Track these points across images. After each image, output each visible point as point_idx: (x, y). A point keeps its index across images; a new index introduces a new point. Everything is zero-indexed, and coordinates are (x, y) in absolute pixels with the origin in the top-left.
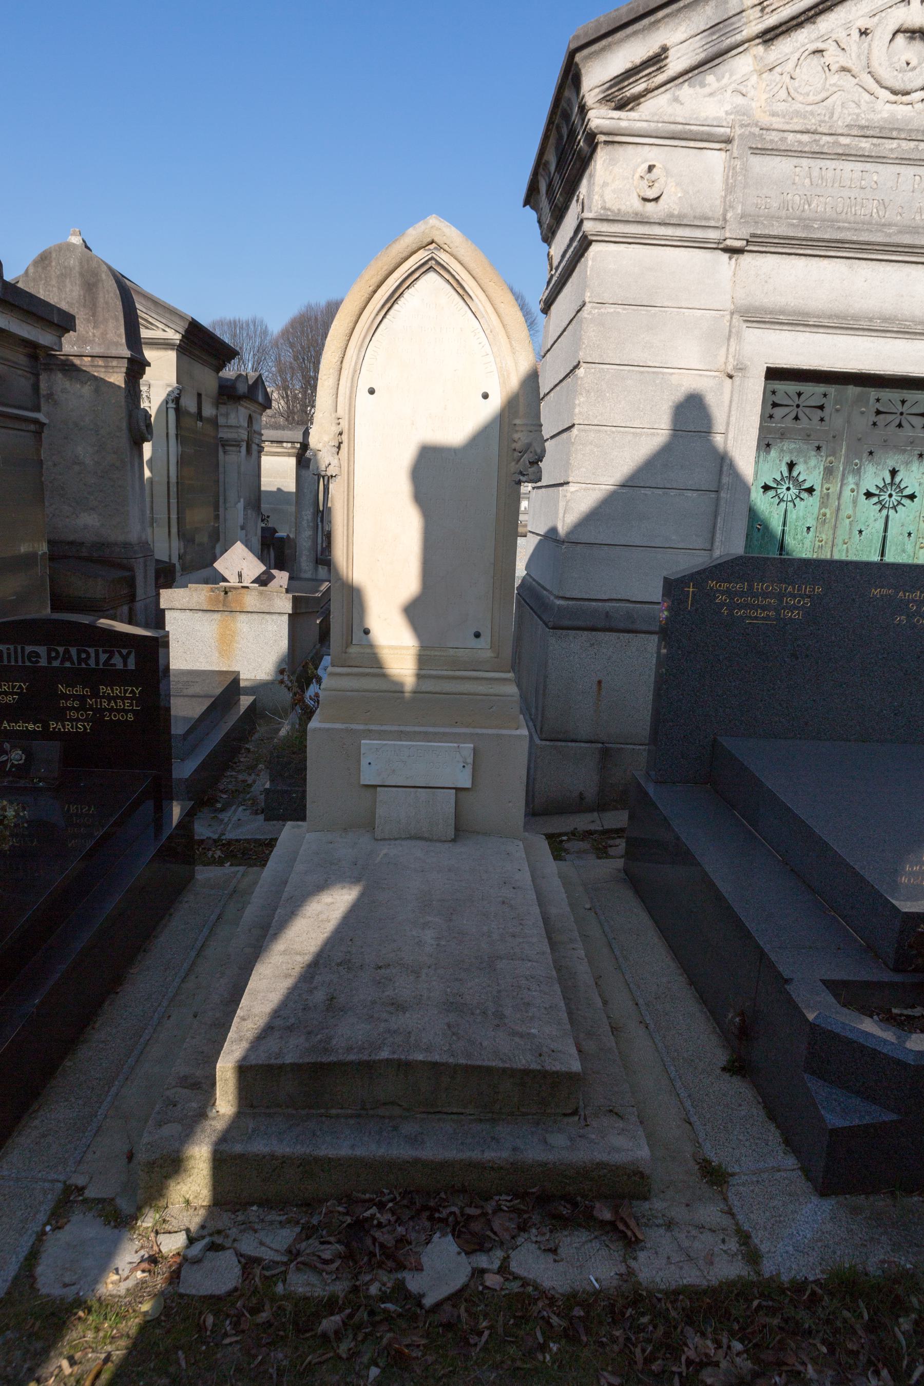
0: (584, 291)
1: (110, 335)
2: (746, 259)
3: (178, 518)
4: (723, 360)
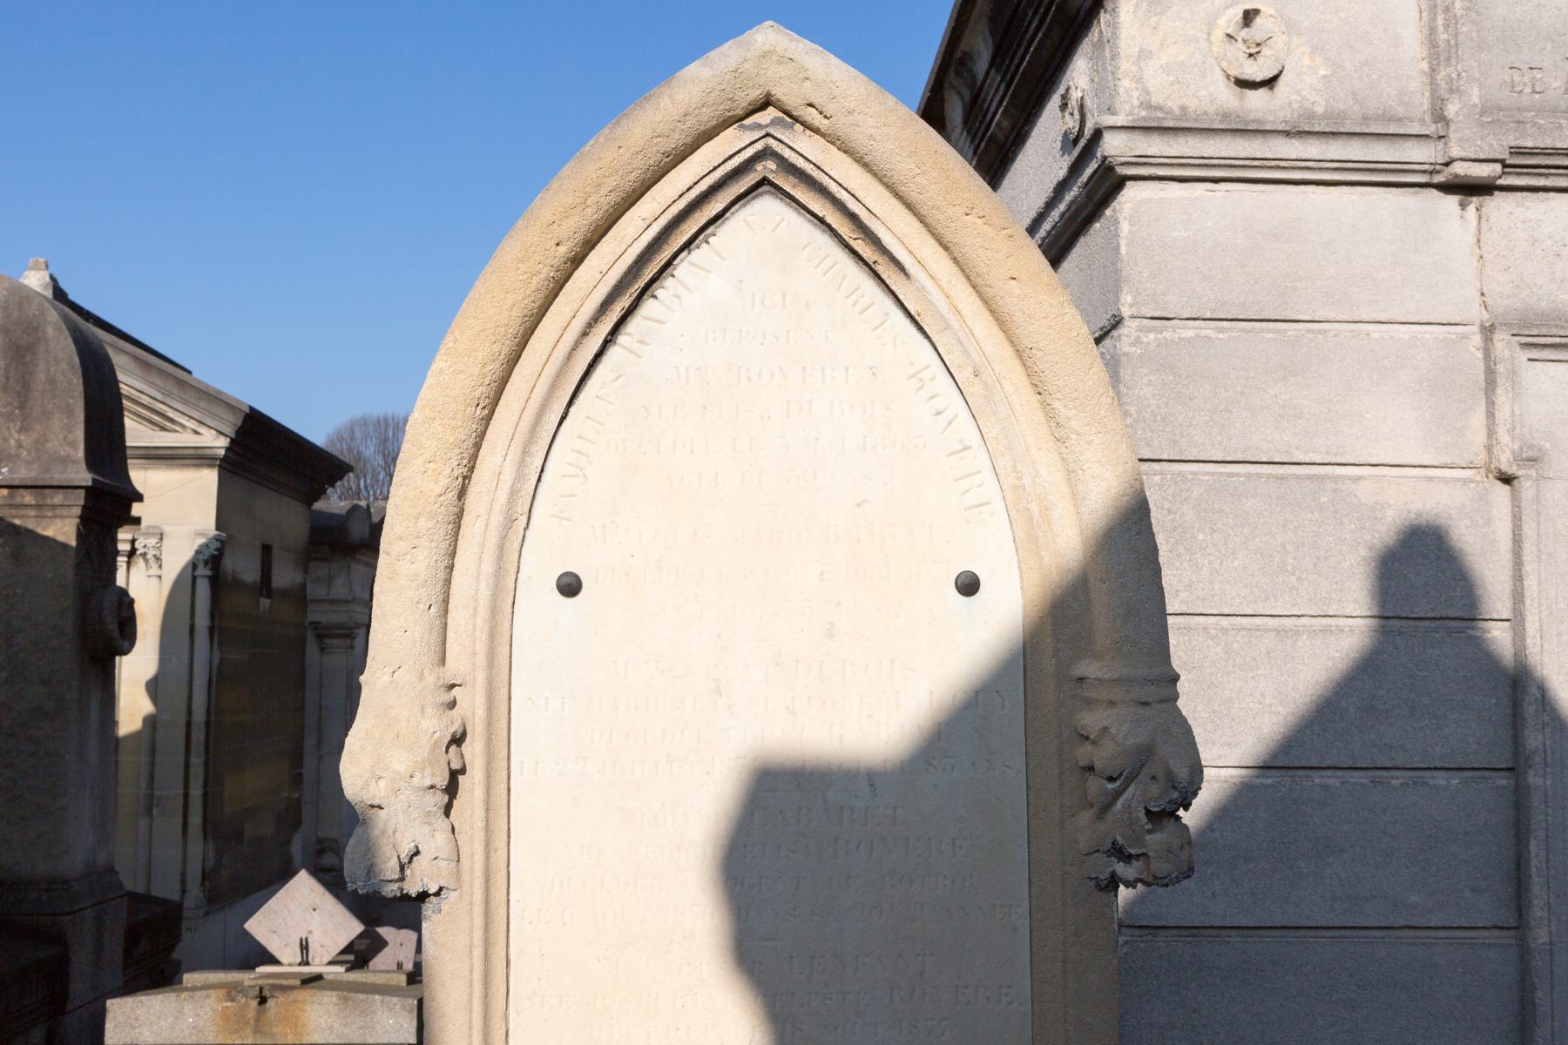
0: (1117, 290)
1: (55, 445)
2: (1498, 204)
3: (205, 795)
4: (1481, 438)
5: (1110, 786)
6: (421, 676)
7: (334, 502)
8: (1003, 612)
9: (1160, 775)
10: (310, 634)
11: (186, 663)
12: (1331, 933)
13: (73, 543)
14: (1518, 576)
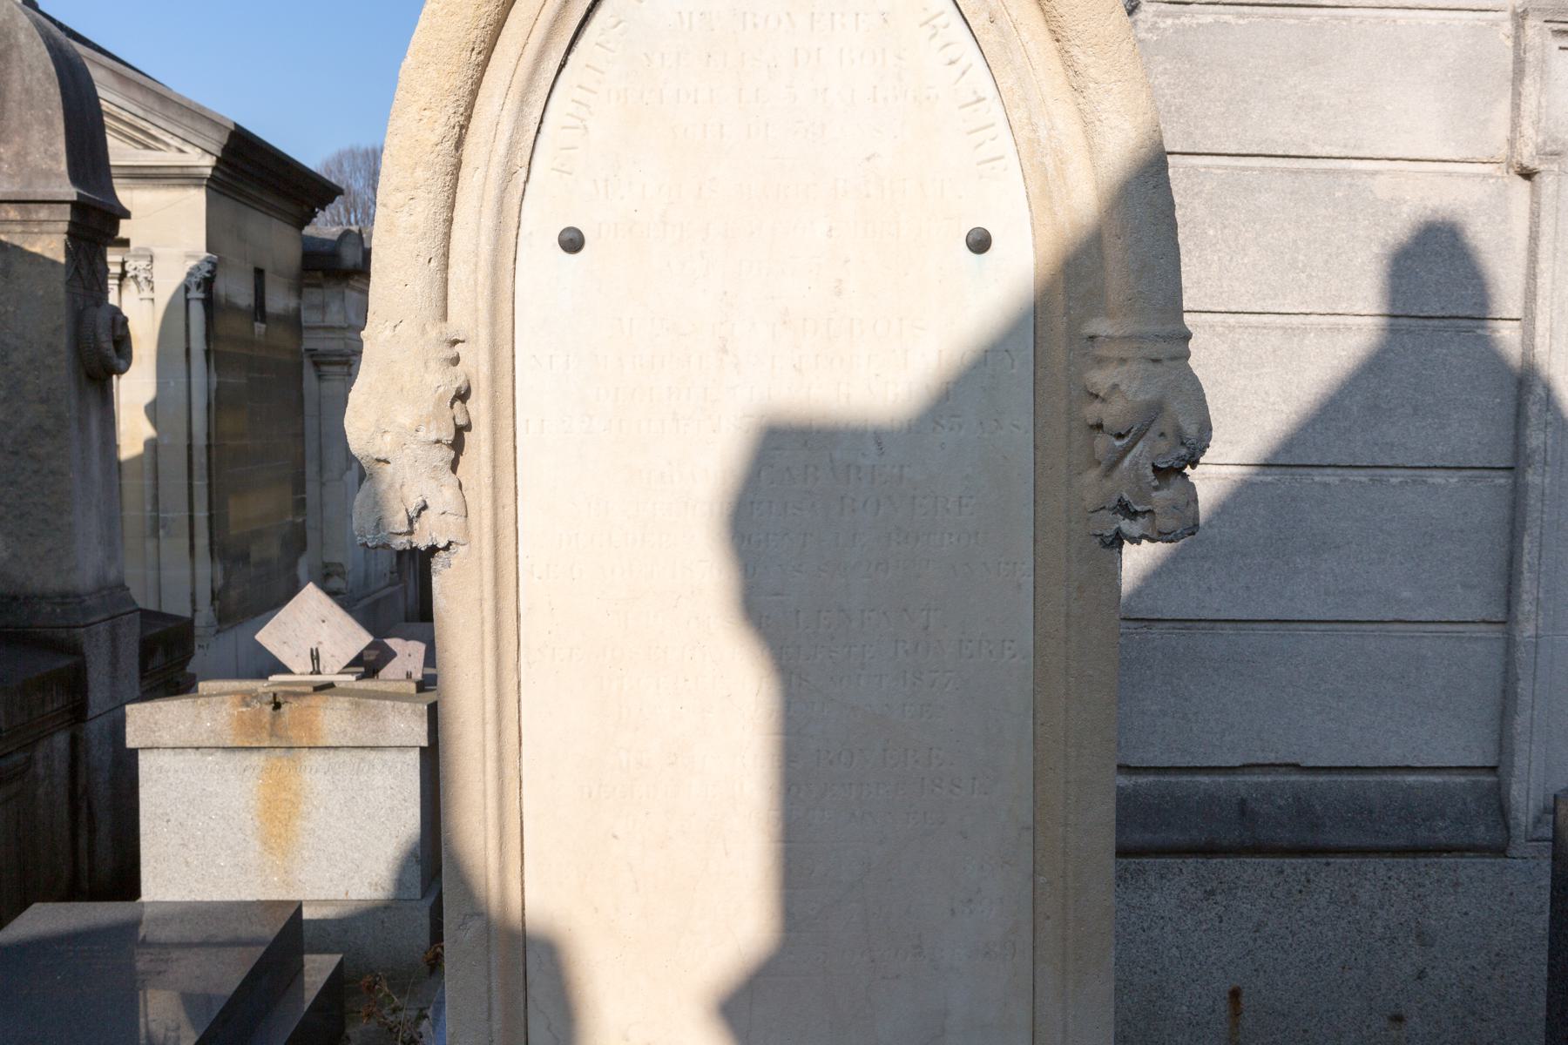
1: (36, 157)
3: (210, 518)
4: (1503, 132)
5: (1118, 443)
6: (423, 331)
7: (325, 226)
8: (1016, 268)
9: (1168, 430)
10: (307, 363)
11: (183, 388)
12: (1323, 626)
13: (62, 260)
14: (1532, 275)
